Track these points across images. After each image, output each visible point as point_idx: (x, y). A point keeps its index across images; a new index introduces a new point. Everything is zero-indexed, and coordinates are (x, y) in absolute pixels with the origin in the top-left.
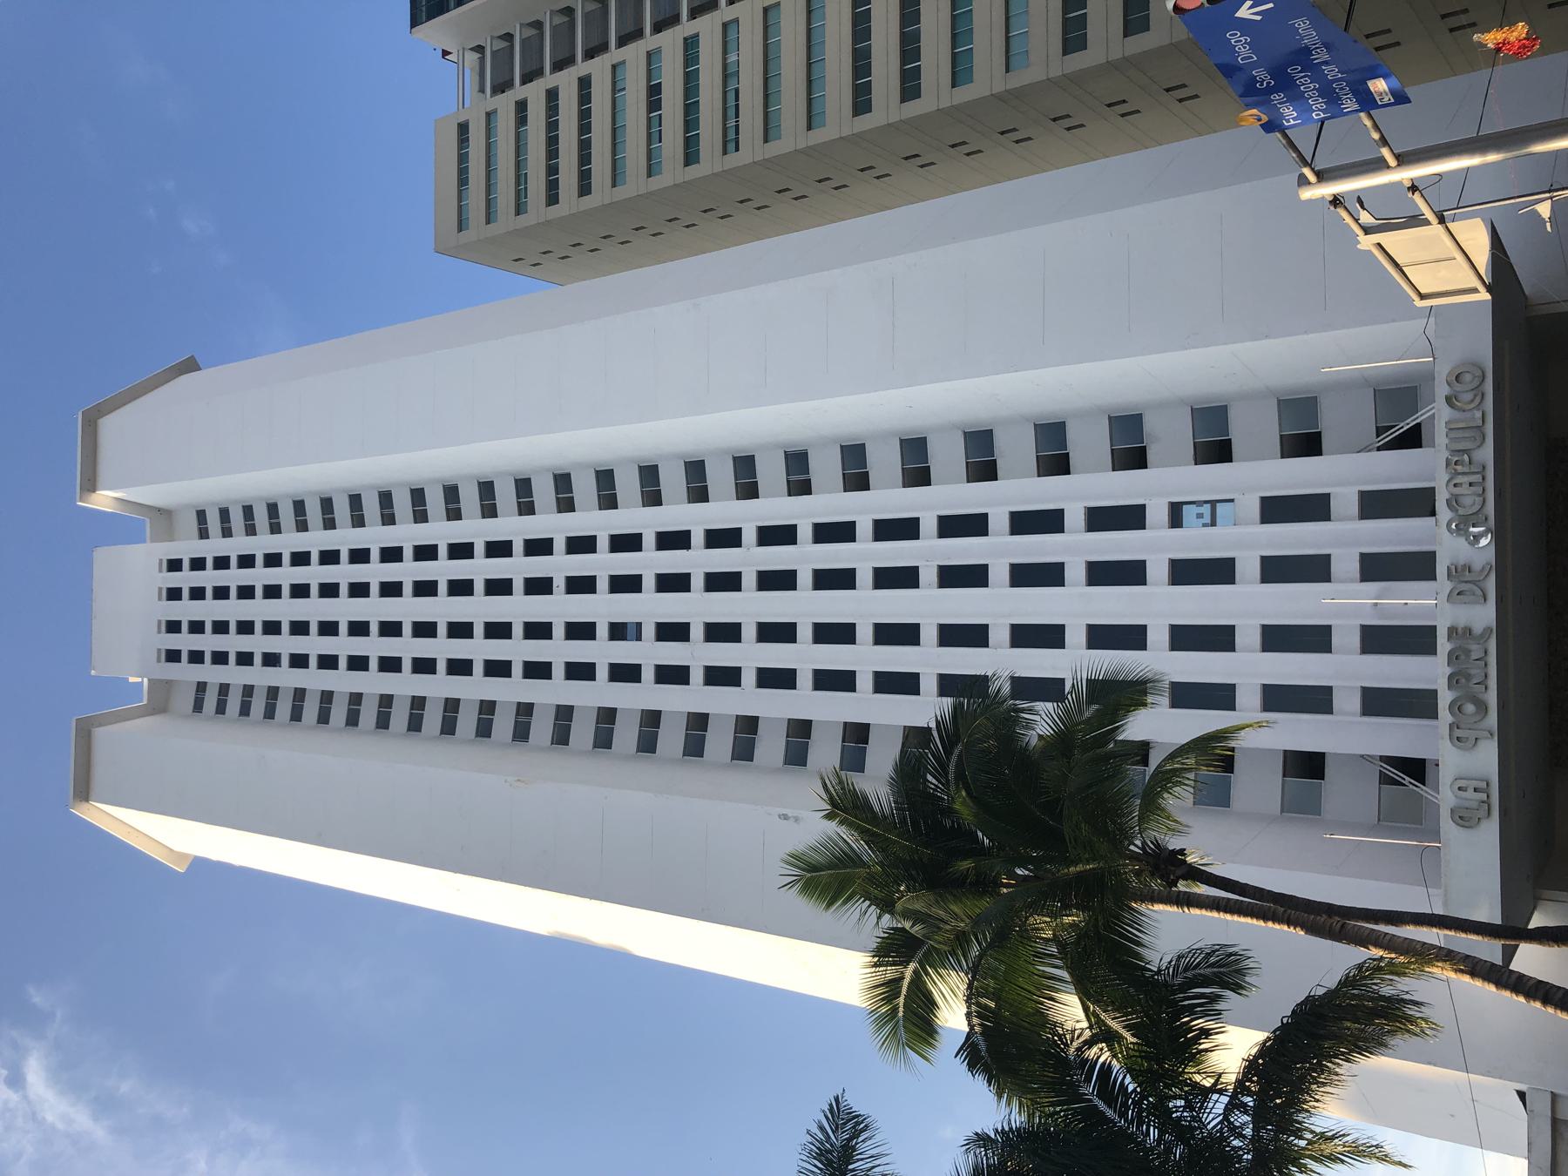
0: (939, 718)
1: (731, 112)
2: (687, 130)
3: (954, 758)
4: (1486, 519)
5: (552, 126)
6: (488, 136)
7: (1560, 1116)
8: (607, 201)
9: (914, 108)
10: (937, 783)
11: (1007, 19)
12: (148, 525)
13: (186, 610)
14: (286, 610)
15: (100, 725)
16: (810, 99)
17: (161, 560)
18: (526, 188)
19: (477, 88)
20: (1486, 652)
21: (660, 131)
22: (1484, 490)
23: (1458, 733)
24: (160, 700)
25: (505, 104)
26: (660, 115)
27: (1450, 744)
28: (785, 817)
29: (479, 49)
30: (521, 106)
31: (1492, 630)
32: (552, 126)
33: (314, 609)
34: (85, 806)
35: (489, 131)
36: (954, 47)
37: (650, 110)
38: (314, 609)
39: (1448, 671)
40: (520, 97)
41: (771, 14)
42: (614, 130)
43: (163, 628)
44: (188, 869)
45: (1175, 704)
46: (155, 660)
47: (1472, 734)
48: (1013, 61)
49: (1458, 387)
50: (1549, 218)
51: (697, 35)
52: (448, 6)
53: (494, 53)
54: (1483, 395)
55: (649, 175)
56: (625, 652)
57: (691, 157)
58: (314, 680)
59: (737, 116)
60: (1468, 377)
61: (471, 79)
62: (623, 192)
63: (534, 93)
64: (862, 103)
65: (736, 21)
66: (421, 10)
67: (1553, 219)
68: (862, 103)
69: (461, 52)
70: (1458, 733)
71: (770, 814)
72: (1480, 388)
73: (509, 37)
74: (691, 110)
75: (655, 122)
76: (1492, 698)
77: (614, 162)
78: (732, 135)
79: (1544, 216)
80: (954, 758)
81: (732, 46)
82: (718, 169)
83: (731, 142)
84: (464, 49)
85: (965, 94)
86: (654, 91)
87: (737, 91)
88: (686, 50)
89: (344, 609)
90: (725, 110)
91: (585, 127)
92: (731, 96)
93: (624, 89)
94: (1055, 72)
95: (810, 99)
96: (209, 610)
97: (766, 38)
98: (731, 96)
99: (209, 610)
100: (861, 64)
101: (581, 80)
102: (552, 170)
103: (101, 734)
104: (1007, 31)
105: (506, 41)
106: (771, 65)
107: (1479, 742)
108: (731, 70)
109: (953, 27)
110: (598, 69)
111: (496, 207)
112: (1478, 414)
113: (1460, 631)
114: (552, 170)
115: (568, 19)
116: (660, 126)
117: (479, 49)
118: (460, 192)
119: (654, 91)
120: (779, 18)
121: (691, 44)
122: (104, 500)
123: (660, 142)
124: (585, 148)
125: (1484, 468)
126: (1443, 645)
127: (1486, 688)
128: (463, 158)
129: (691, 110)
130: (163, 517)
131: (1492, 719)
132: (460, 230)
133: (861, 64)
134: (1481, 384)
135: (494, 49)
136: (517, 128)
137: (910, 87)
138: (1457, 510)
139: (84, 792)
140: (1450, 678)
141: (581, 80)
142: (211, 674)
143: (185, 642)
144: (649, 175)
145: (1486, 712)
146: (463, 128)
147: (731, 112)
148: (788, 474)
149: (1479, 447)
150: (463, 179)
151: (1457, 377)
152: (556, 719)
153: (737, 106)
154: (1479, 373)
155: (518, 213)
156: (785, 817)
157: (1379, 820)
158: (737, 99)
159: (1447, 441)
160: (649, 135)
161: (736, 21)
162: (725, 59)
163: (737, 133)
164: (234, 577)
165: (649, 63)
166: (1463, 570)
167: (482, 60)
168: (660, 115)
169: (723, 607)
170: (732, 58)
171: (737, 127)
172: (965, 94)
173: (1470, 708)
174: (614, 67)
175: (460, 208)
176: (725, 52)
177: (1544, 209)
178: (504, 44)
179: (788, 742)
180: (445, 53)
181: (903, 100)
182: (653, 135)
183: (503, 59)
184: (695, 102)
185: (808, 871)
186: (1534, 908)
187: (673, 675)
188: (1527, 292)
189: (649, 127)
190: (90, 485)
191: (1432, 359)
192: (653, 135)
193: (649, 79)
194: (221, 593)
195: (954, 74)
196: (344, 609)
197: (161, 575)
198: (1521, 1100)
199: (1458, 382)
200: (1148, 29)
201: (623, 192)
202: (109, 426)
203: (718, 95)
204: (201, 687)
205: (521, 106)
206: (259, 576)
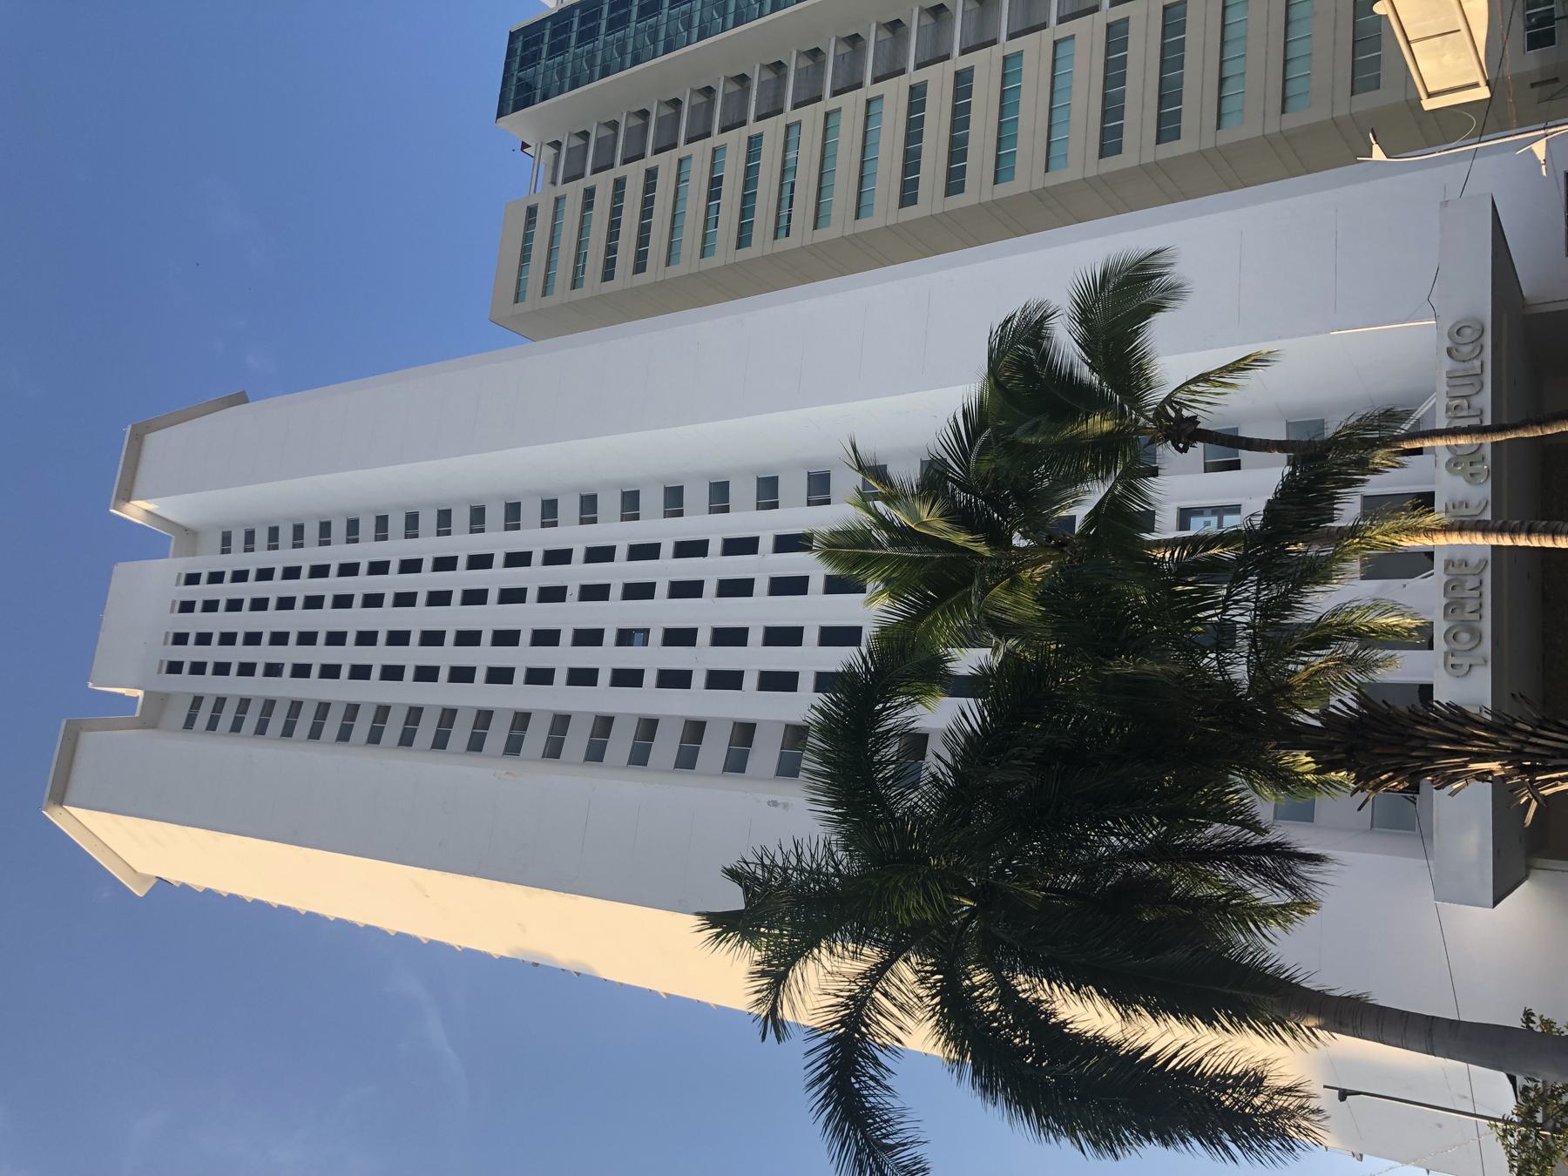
0: (966, 406)
1: (786, 203)
2: (742, 217)
3: (976, 449)
4: (1483, 458)
5: (616, 212)
6: (555, 218)
8: (660, 278)
9: (957, 201)
10: (960, 472)
11: (1050, 126)
13: (198, 622)
14: (296, 620)
15: (90, 730)
16: (861, 193)
17: (167, 633)
19: (549, 179)
20: (1481, 583)
21: (717, 218)
22: (1481, 595)
23: (1452, 660)
24: (152, 715)
25: (574, 191)
26: (719, 204)
27: (1444, 672)
28: (775, 804)
29: (556, 145)
30: (589, 193)
31: (1487, 562)
32: (616, 212)
33: (325, 620)
34: (58, 810)
35: (556, 215)
36: (999, 148)
37: (710, 199)
38: (325, 620)
39: (1444, 601)
40: (588, 185)
42: (674, 217)
43: (170, 639)
46: (156, 670)
47: (1465, 661)
48: (1052, 164)
49: (1459, 339)
51: (761, 135)
52: (533, 101)
53: (569, 150)
54: (1482, 347)
55: (702, 256)
56: (629, 657)
57: (743, 240)
58: (314, 689)
59: (791, 206)
60: (1467, 331)
61: (545, 174)
62: (676, 271)
63: (603, 183)
64: (908, 195)
65: (799, 123)
66: (508, 104)
67: (1548, 162)
68: (908, 195)
69: (539, 146)
70: (1452, 660)
71: (759, 801)
72: (1480, 340)
73: (585, 135)
74: (748, 199)
75: (713, 210)
76: (1486, 626)
77: (670, 244)
78: (784, 222)
79: (1540, 158)
80: (976, 449)
81: (792, 145)
82: (768, 251)
83: (782, 228)
84: (542, 143)
85: (1006, 190)
86: (716, 182)
87: (793, 184)
88: (749, 146)
89: (354, 620)
90: (780, 200)
91: (646, 212)
92: (787, 189)
93: (687, 181)
94: (1091, 172)
95: (861, 193)
96: (219, 622)
97: (825, 138)
98: (787, 189)
99: (219, 622)
100: (911, 163)
101: (648, 171)
102: (611, 250)
103: (89, 740)
104: (1049, 137)
105: (582, 139)
106: (828, 162)
107: (1473, 668)
108: (790, 165)
109: (999, 132)
110: (666, 163)
111: (554, 281)
112: (1477, 363)
113: (1457, 563)
114: (611, 250)
116: (718, 213)
117: (556, 145)
118: (521, 267)
119: (716, 182)
120: (835, 165)
121: (754, 142)
122: (135, 511)
123: (716, 227)
124: (644, 230)
125: (1482, 412)
127: (1481, 617)
128: (528, 238)
129: (748, 199)
130: (189, 536)
131: (1487, 646)
132: (516, 301)
133: (911, 163)
134: (1480, 337)
135: (571, 146)
136: (583, 211)
137: (955, 182)
138: (1456, 451)
139: (59, 799)
140: (1446, 607)
141: (648, 171)
142: (210, 685)
143: (190, 653)
144: (702, 256)
145: (1480, 641)
146: (532, 212)
147: (786, 203)
148: (809, 494)
149: (1477, 393)
150: (525, 257)
151: (1458, 332)
152: (550, 733)
153: (791, 198)
154: (1478, 327)
155: (574, 287)
156: (775, 804)
157: (1372, 826)
158: (792, 191)
159: (1447, 389)
160: (706, 221)
161: (799, 123)
162: (784, 156)
163: (789, 221)
164: (251, 589)
165: (713, 158)
166: (1460, 565)
167: (557, 157)
168: (719, 204)
169: (733, 612)
170: (791, 155)
171: (790, 216)
172: (1006, 190)
173: (1465, 636)
174: (680, 161)
175: (519, 281)
176: (786, 150)
177: (1540, 149)
178: (581, 142)
179: (782, 754)
180: (524, 146)
181: (947, 194)
182: (711, 209)
183: (577, 156)
185: (828, 546)
186: (1526, 877)
187: (675, 679)
188: (1525, 293)
189: (707, 213)
190: (126, 495)
192: (710, 220)
193: (712, 171)
194: (228, 639)
195: (996, 173)
196: (354, 620)
197: (178, 588)
198: (1511, 1083)
200: (1179, 138)
201: (676, 271)
204: (197, 701)
205: (589, 193)
206: (276, 588)
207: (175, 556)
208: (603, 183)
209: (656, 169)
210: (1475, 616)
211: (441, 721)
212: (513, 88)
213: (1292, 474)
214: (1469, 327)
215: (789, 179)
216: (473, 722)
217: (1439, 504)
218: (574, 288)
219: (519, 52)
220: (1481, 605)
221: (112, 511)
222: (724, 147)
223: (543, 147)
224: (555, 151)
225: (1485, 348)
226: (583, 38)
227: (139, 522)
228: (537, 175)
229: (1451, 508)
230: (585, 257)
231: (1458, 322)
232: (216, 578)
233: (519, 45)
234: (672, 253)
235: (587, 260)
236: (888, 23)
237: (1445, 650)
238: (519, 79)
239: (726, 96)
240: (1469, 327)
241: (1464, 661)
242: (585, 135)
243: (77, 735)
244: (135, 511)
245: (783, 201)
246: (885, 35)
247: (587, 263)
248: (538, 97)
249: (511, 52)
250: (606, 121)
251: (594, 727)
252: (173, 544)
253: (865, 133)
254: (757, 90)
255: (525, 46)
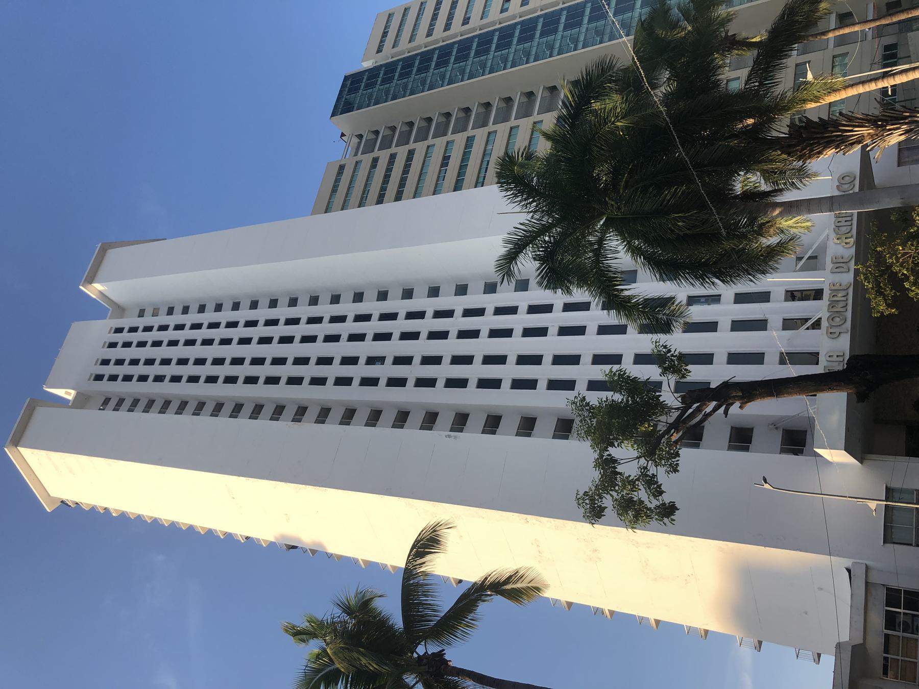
1: (483, 170)
2: (458, 176)
6: (354, 171)
7: (871, 580)
12: (110, 312)
13: (120, 353)
18: (367, 196)
22: (847, 299)
26: (446, 169)
29: (360, 137)
30: (375, 161)
31: (851, 284)
32: (389, 170)
34: (14, 449)
37: (442, 166)
41: (513, 130)
44: (53, 511)
45: (685, 331)
50: (875, 510)
51: (474, 136)
54: (854, 186)
59: (486, 172)
65: (496, 132)
66: (341, 104)
69: (351, 135)
72: (853, 183)
75: (443, 172)
76: (849, 314)
81: (490, 142)
84: (353, 135)
86: (446, 160)
87: (488, 162)
110: (420, 148)
115: (409, 129)
116: (445, 174)
117: (360, 137)
118: (331, 195)
119: (446, 160)
121: (470, 141)
122: (95, 289)
126: (826, 294)
128: (337, 181)
130: (120, 310)
131: (849, 324)
136: (370, 169)
146: (342, 168)
147: (483, 170)
150: (334, 190)
151: (842, 178)
153: (487, 168)
158: (488, 165)
160: (438, 177)
162: (486, 147)
163: (484, 179)
167: (359, 143)
170: (489, 147)
171: (485, 177)
176: (487, 144)
178: (374, 136)
184: (465, 165)
189: (439, 173)
190: (91, 280)
191: (831, 177)
197: (109, 335)
199: (832, 320)
202: (113, 255)
203: (479, 161)
205: (375, 161)
207: (110, 319)
208: (384, 156)
209: (414, 150)
210: (844, 309)
211: (253, 411)
212: (342, 103)
213: (767, 42)
214: (848, 176)
215: (486, 159)
216: (273, 410)
217: (822, 359)
218: (360, 207)
219: (348, 86)
220: (847, 304)
221: (81, 287)
222: (453, 141)
223: (353, 138)
224: (359, 140)
225: (856, 179)
226: (384, 81)
227: (94, 297)
228: (347, 151)
229: (834, 259)
230: (368, 192)
231: (843, 174)
232: (133, 330)
233: (349, 83)
234: (468, 10)
235: (369, 193)
236: (549, 87)
237: (825, 365)
238: (346, 99)
239: (457, 119)
240: (848, 176)
241: (837, 330)
242: (377, 133)
243: (34, 409)
244: (95, 289)
245: (482, 169)
246: (547, 94)
247: (369, 195)
248: (355, 108)
249: (343, 86)
250: (390, 126)
251: (344, 414)
252: (110, 312)
253: (531, 139)
254: (474, 120)
255: (352, 83)
